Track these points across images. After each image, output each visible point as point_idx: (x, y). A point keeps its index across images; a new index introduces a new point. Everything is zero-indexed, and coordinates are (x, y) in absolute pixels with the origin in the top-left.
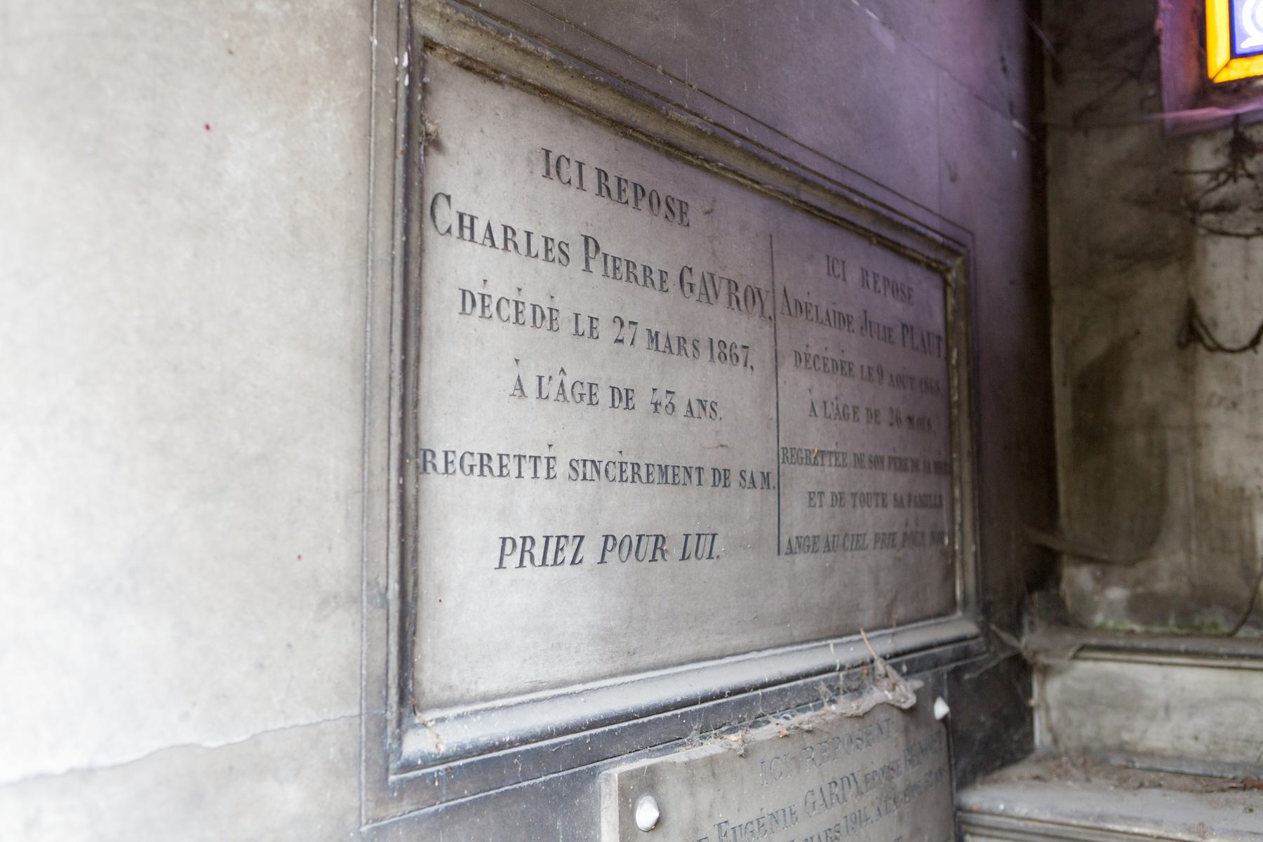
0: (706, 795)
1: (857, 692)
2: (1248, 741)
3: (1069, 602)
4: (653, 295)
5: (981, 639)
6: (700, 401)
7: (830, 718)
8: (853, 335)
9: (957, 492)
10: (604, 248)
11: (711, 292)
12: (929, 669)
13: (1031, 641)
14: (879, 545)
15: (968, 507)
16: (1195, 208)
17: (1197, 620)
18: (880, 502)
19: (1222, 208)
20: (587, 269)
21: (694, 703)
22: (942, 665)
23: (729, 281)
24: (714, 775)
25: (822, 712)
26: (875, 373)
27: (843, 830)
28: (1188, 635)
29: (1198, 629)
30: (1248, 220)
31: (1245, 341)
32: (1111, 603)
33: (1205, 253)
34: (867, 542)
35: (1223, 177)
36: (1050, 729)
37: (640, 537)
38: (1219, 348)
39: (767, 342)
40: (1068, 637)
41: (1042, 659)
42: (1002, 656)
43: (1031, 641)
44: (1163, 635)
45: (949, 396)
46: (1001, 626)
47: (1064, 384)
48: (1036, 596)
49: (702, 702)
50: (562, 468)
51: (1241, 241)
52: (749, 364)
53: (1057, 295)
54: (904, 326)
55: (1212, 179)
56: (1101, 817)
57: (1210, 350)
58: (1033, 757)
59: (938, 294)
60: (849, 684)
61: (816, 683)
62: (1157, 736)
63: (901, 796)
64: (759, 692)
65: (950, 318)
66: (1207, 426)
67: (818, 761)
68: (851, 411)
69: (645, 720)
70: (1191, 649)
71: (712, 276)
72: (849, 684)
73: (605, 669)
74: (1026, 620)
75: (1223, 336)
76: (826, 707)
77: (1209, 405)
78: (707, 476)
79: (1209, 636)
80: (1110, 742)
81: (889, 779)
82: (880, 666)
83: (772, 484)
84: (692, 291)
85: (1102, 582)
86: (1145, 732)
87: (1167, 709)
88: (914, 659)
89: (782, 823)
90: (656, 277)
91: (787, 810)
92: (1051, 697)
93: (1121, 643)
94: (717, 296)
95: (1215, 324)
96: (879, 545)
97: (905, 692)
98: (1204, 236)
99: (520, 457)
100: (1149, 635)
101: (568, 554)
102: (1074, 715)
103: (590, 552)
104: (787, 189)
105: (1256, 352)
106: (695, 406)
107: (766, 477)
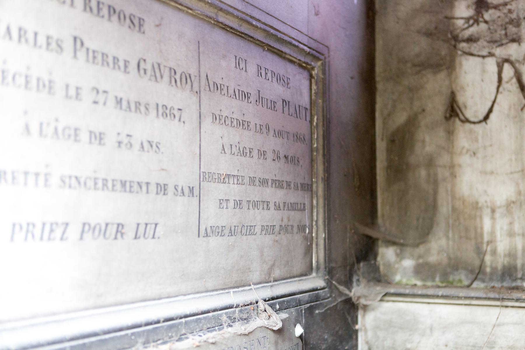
1: (246, 320)
3: (382, 268)
4: (120, 75)
6: (149, 142)
7: (227, 335)
8: (250, 105)
9: (315, 202)
10: (87, 44)
11: (158, 75)
13: (358, 291)
14: (264, 232)
15: (321, 211)
16: (456, 39)
17: (451, 278)
18: (265, 206)
19: (470, 40)
20: (75, 56)
21: (140, 326)
23: (170, 69)
25: (222, 332)
26: (264, 129)
28: (445, 287)
29: (452, 283)
30: (484, 47)
31: (481, 117)
32: (405, 269)
33: (461, 65)
34: (256, 230)
35: (471, 22)
36: (367, 343)
37: (107, 225)
38: (467, 121)
39: (195, 107)
40: (378, 288)
41: (363, 301)
43: (358, 291)
44: (432, 287)
45: (312, 144)
46: (340, 283)
47: (382, 140)
48: (362, 264)
50: (55, 180)
51: (480, 59)
52: (182, 120)
53: (380, 86)
54: (284, 101)
55: (466, 23)
57: (462, 121)
59: (307, 83)
60: (241, 315)
61: (221, 315)
64: (183, 320)
65: (313, 97)
66: (460, 166)
68: (248, 151)
69: (107, 336)
70: (445, 294)
71: (159, 65)
72: (241, 315)
74: (355, 279)
75: (469, 114)
76: (225, 329)
77: (461, 153)
78: (153, 188)
79: (456, 287)
82: (262, 305)
83: (195, 195)
84: (145, 73)
85: (400, 256)
86: (419, 343)
88: (284, 301)
90: (121, 64)
93: (407, 291)
94: (162, 77)
95: (466, 107)
96: (264, 232)
97: (276, 321)
98: (461, 55)
99: (26, 173)
100: (425, 287)
101: (58, 233)
102: (381, 334)
103: (73, 232)
104: (210, 14)
105: (486, 123)
106: (146, 145)
107: (191, 190)
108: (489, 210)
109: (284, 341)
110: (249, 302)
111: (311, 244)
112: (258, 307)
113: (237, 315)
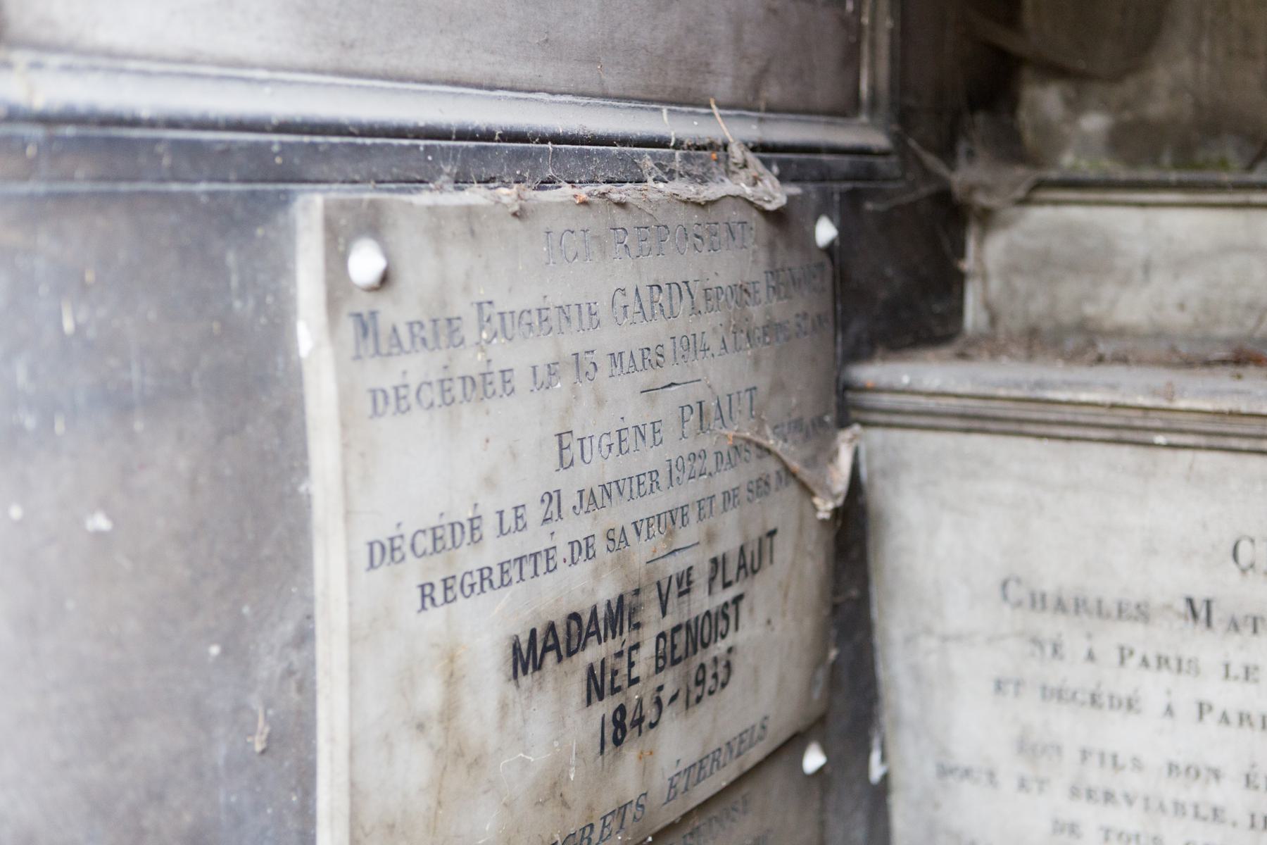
0: (459, 259)
2: (1250, 306)
5: (894, 159)
12: (813, 180)
13: (969, 175)
22: (831, 180)
24: (472, 233)
27: (668, 352)
36: (988, 306)
40: (1020, 171)
41: (981, 199)
42: (924, 190)
43: (969, 175)
49: (458, 139)
56: (1040, 385)
58: (958, 345)
61: (640, 156)
62: (1130, 307)
63: (758, 333)
67: (634, 251)
69: (368, 141)
73: (306, 58)
74: (962, 147)
80: (1067, 318)
81: (742, 304)
85: (1075, 107)
87: (1147, 268)
88: (790, 161)
89: (575, 323)
91: (585, 309)
92: (989, 257)
97: (774, 193)
102: (1020, 283)
108: (1232, 672)
109: (789, 246)
110: (707, 141)
111: (857, 45)
112: (727, 157)
113: (677, 164)
